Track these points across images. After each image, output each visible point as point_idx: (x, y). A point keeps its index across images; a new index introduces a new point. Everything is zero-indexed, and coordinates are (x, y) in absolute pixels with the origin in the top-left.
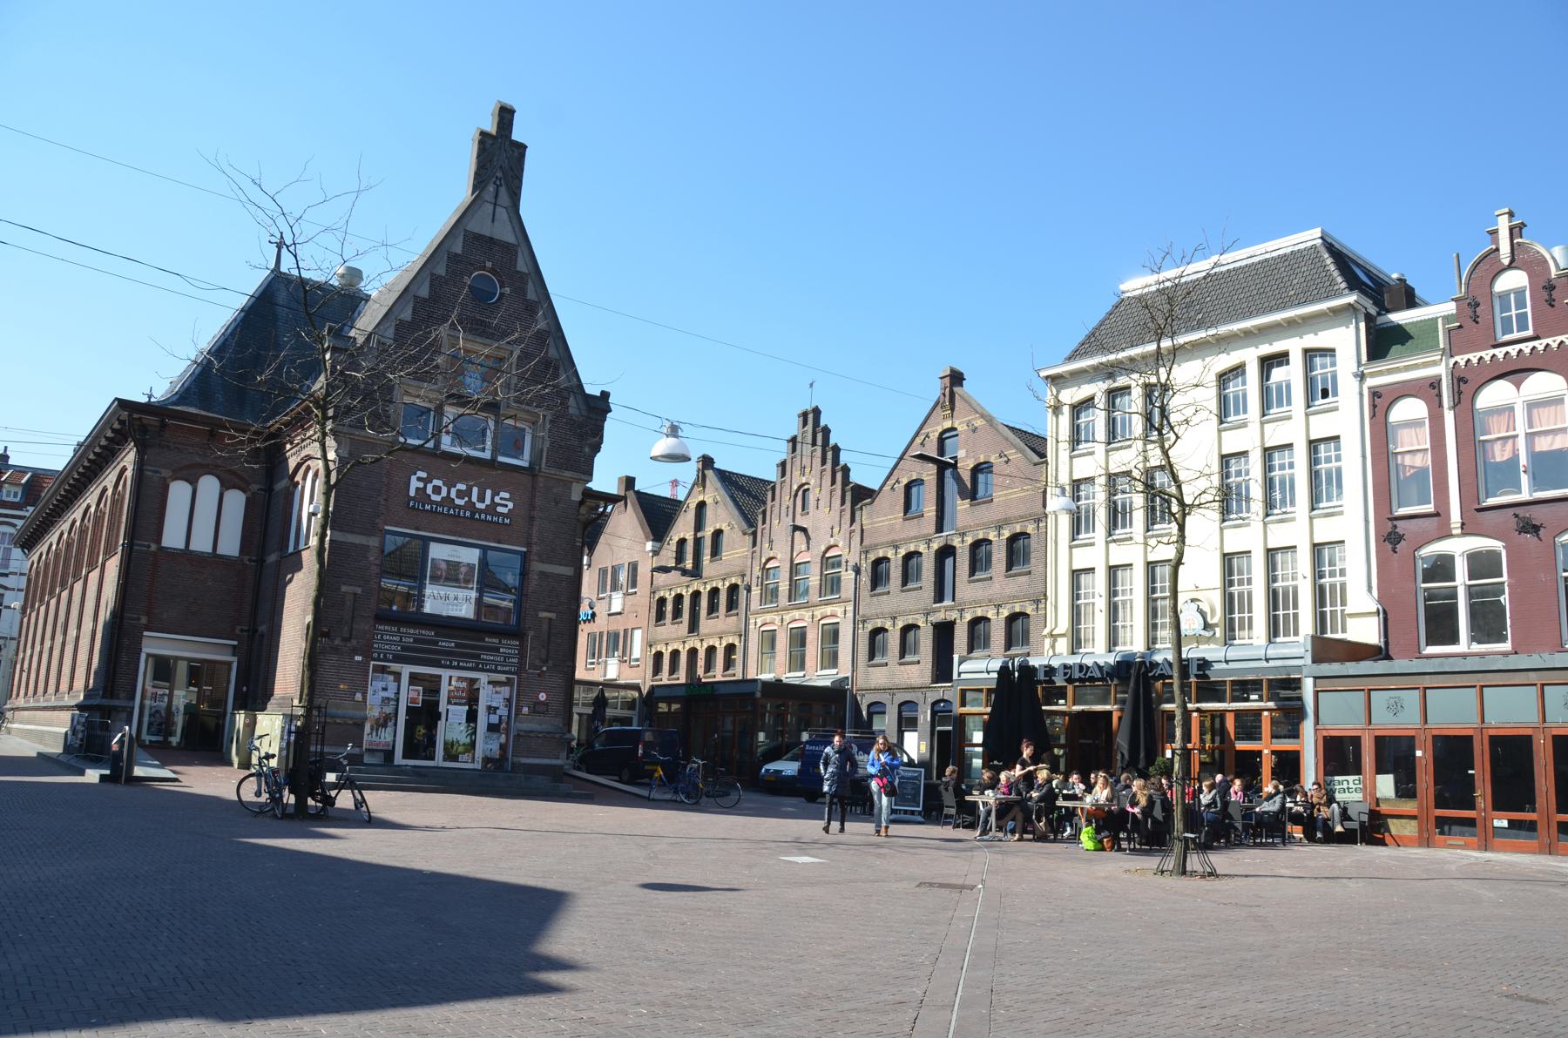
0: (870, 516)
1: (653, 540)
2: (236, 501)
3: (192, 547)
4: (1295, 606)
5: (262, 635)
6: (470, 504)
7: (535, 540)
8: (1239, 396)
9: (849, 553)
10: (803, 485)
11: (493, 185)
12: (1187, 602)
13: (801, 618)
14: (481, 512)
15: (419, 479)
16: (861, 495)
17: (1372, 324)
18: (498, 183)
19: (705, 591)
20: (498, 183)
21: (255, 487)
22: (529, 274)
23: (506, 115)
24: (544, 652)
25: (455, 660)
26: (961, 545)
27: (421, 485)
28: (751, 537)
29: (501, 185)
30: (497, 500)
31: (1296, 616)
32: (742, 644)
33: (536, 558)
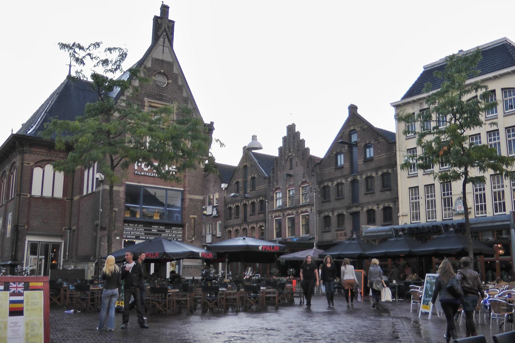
2: (60, 176)
3: (44, 195)
7: (187, 185)
10: (290, 156)
18: (164, 37)
20: (164, 37)
22: (179, 74)
23: (165, 9)
24: (192, 232)
25: (147, 236)
29: (165, 38)
33: (188, 193)
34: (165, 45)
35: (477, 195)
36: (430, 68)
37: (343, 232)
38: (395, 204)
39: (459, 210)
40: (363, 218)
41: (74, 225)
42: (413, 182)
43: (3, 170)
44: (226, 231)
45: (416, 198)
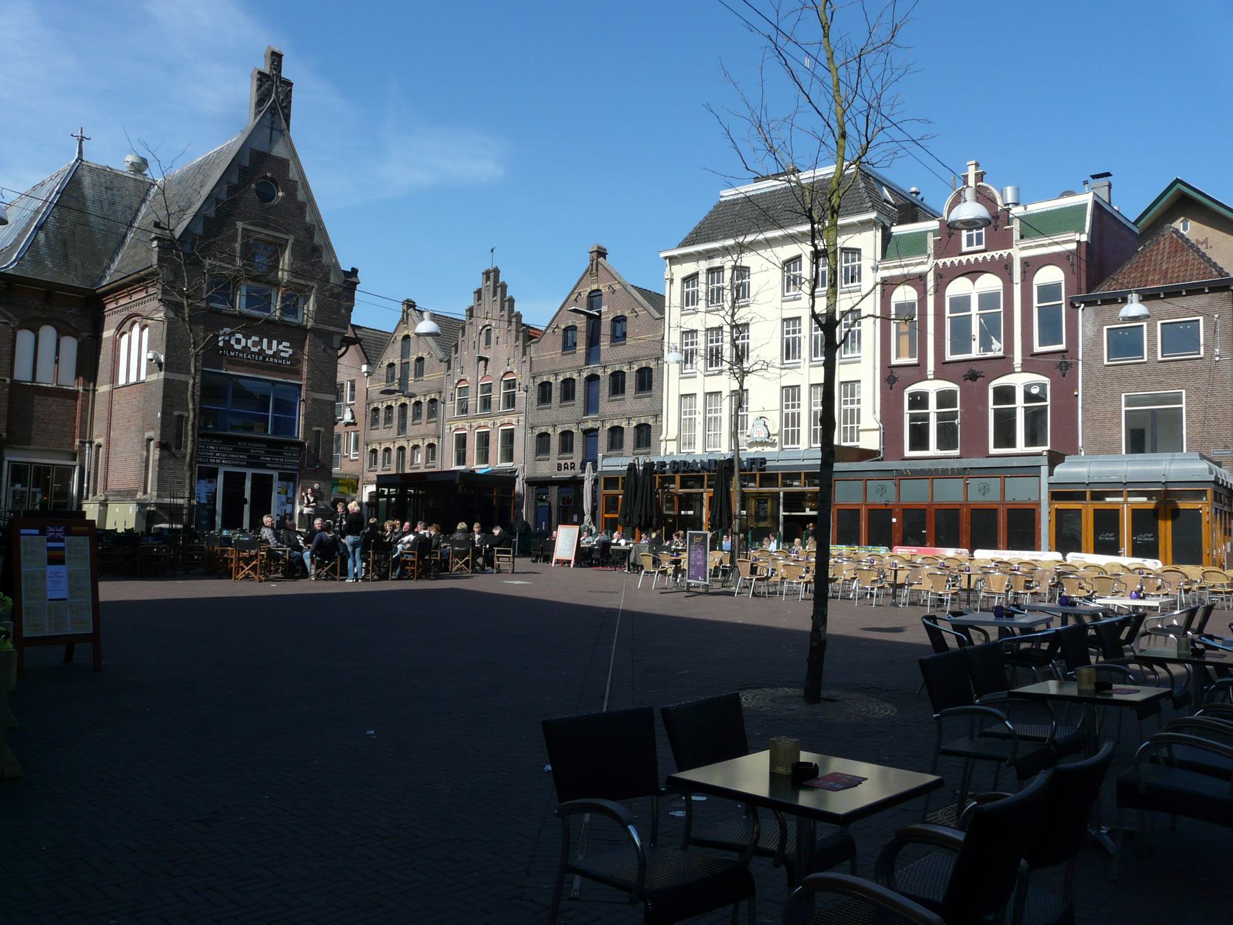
0: (537, 351)
1: (366, 364)
6: (262, 350)
9: (522, 377)
13: (486, 424)
14: (270, 356)
16: (528, 335)
18: (273, 112)
21: (85, 334)
23: (276, 58)
28: (446, 364)
30: (281, 347)
32: (441, 444)
36: (731, 198)
37: (569, 462)
38: (656, 421)
40: (603, 440)
42: (687, 387)
44: (367, 449)
45: (793, 406)
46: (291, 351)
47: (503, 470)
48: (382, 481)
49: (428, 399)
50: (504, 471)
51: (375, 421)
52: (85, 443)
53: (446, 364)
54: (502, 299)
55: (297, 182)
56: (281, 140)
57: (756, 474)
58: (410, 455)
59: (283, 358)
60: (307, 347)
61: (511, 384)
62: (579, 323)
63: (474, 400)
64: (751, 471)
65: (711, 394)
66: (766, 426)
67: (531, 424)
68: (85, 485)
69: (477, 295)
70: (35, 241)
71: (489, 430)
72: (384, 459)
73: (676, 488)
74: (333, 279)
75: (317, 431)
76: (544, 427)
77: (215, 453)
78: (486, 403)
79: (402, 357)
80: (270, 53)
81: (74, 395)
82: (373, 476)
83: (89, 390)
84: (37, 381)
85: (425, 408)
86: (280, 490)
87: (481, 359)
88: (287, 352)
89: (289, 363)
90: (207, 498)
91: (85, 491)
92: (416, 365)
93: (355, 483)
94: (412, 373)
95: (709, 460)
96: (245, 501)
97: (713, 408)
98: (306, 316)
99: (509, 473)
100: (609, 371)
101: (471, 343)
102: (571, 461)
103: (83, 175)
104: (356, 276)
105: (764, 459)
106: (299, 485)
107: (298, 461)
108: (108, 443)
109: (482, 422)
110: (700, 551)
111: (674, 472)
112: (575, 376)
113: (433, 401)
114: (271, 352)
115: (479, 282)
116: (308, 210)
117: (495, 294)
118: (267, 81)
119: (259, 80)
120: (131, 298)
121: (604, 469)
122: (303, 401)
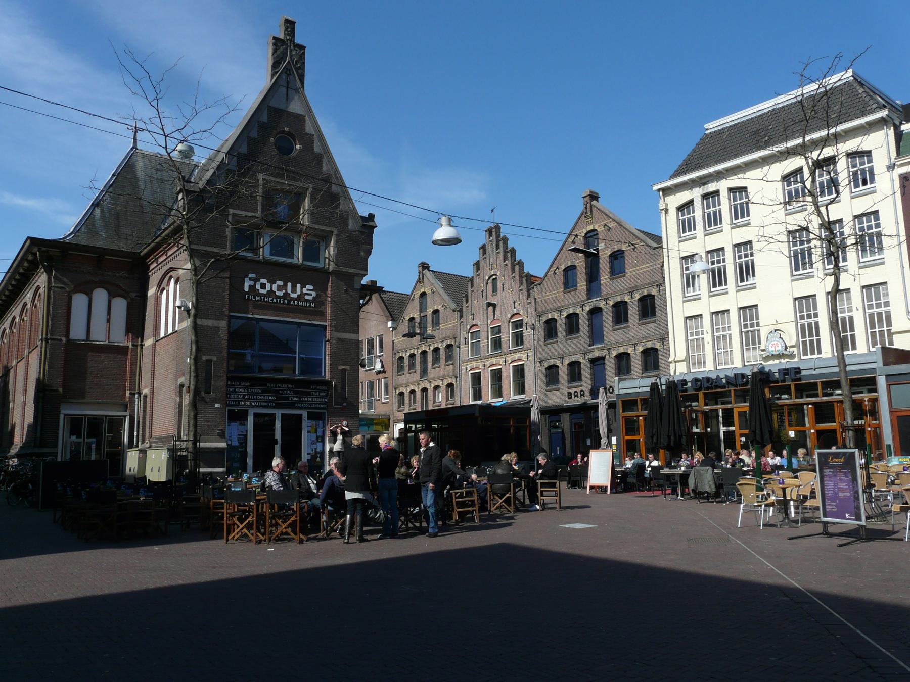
0: (540, 292)
1: (391, 320)
4: (818, 335)
5: (146, 396)
6: (286, 294)
8: (798, 189)
9: (528, 316)
10: (492, 276)
11: (285, 75)
12: (771, 332)
13: (498, 362)
14: (294, 299)
15: (250, 279)
16: (530, 281)
17: (897, 131)
18: (288, 72)
19: (430, 350)
21: (133, 295)
23: (290, 25)
26: (605, 306)
27: (252, 283)
28: (459, 313)
30: (305, 290)
31: (819, 341)
32: (458, 383)
34: (289, 86)
35: (803, 326)
36: (716, 129)
37: (578, 390)
38: (663, 344)
39: (773, 349)
40: (610, 366)
41: (146, 387)
42: (692, 309)
43: (23, 301)
44: (396, 392)
46: (314, 294)
47: (516, 402)
48: (409, 419)
49: (445, 345)
50: (518, 403)
51: (400, 368)
52: (134, 394)
53: (459, 313)
54: (504, 251)
55: (313, 135)
56: (296, 97)
57: (790, 385)
58: (432, 395)
59: (307, 301)
60: (329, 289)
61: (518, 325)
62: (578, 263)
63: (486, 342)
64: (785, 382)
65: (717, 313)
66: (782, 339)
67: (540, 358)
68: (135, 434)
69: (481, 250)
70: (92, 216)
71: (501, 367)
72: (410, 400)
73: (700, 405)
74: (351, 225)
75: (343, 370)
76: (552, 360)
77: (244, 396)
78: (497, 344)
79: (421, 311)
80: (283, 21)
81: (124, 350)
82: (401, 416)
83: (137, 346)
84: (91, 339)
85: (442, 353)
86: (310, 429)
87: (489, 304)
88: (311, 295)
89: (313, 305)
90: (238, 440)
91: (135, 439)
92: (432, 317)
93: (386, 421)
94: (429, 325)
95: (735, 374)
96: (276, 442)
97: (721, 327)
98: (327, 260)
99: (523, 404)
100: (611, 302)
101: (480, 292)
102: (581, 389)
103: (137, 161)
104: (374, 221)
105: (799, 368)
106: (328, 423)
107: (326, 400)
108: (152, 392)
109: (494, 361)
110: (843, 478)
111: (696, 390)
112: (578, 311)
113: (449, 346)
114: (294, 296)
115: (483, 239)
116: (325, 160)
117: (498, 247)
118: (282, 46)
119: (274, 44)
120: (166, 255)
121: (622, 392)
122: (328, 341)
